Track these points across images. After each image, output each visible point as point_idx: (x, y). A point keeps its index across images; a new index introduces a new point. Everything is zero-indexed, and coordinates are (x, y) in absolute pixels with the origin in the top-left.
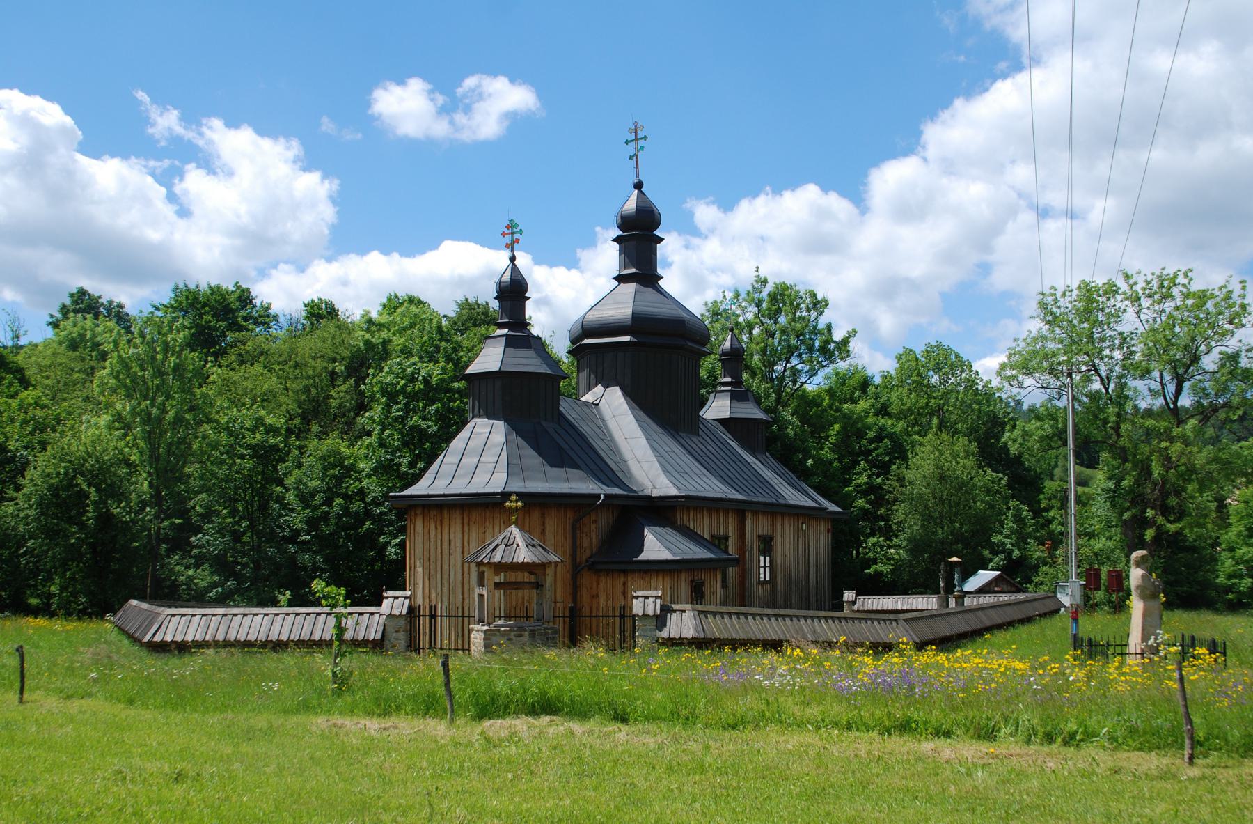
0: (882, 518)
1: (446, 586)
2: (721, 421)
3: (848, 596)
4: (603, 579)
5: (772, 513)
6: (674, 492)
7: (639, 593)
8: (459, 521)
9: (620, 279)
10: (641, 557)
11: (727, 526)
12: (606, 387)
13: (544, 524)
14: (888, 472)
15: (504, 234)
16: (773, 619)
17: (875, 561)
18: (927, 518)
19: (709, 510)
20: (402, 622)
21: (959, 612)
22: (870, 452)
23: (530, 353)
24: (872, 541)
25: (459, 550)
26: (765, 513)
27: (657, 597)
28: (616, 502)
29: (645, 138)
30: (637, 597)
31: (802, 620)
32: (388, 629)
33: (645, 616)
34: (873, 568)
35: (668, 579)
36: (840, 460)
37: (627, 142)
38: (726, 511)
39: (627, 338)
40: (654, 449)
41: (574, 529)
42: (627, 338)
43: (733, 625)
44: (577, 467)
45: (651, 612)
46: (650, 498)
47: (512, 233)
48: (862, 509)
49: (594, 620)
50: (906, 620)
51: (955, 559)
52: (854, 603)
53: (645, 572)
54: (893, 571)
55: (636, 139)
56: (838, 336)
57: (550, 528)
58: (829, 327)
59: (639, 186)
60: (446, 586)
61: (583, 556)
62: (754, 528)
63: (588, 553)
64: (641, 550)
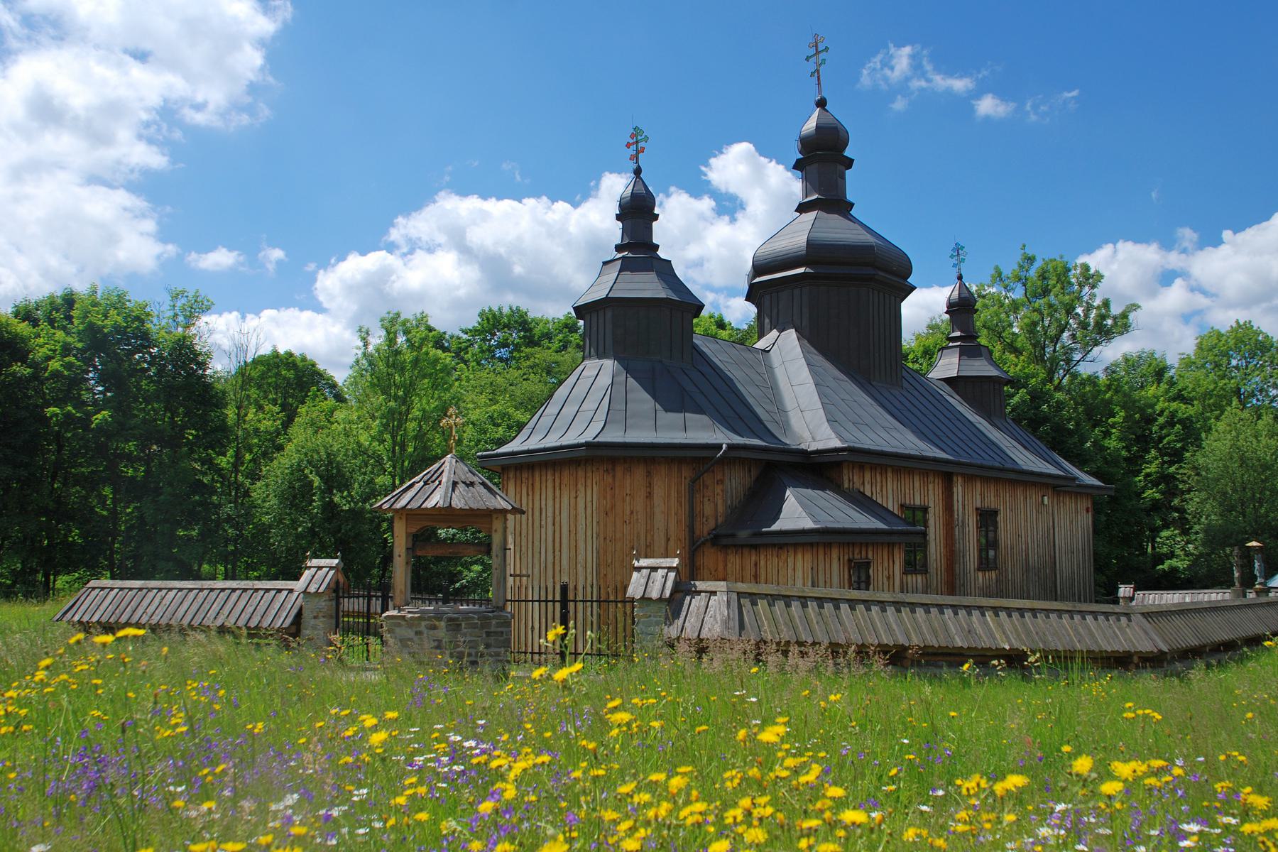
0: (1176, 510)
1: (537, 566)
2: (948, 381)
3: (1124, 590)
4: (731, 558)
5: (997, 480)
6: (836, 443)
7: (644, 562)
8: (550, 478)
9: (802, 208)
10: (776, 527)
11: (927, 494)
12: (781, 331)
13: (650, 485)
14: (1181, 460)
15: (628, 145)
16: (890, 610)
17: (1172, 555)
18: (1227, 508)
19: (897, 471)
20: (323, 604)
21: (1238, 607)
22: (1161, 439)
23: (652, 276)
24: (1165, 533)
25: (550, 520)
26: (986, 480)
27: (670, 569)
28: (743, 454)
29: (826, 49)
30: (639, 569)
31: (948, 613)
32: (306, 613)
33: (645, 599)
34: (1168, 563)
35: (808, 557)
36: (1127, 448)
37: (807, 59)
38: (924, 473)
39: (801, 270)
40: (821, 395)
41: (692, 492)
42: (801, 270)
43: (901, 622)
44: (700, 410)
45: (655, 594)
46: (804, 453)
47: (637, 142)
48: (1153, 500)
49: (543, 598)
50: (1146, 615)
51: (1254, 544)
52: (1132, 599)
53: (781, 546)
54: (1189, 567)
55: (817, 52)
56: (1116, 310)
57: (659, 490)
58: (1106, 304)
59: (821, 104)
60: (537, 566)
61: (704, 529)
62: (968, 499)
63: (712, 524)
64: (776, 517)
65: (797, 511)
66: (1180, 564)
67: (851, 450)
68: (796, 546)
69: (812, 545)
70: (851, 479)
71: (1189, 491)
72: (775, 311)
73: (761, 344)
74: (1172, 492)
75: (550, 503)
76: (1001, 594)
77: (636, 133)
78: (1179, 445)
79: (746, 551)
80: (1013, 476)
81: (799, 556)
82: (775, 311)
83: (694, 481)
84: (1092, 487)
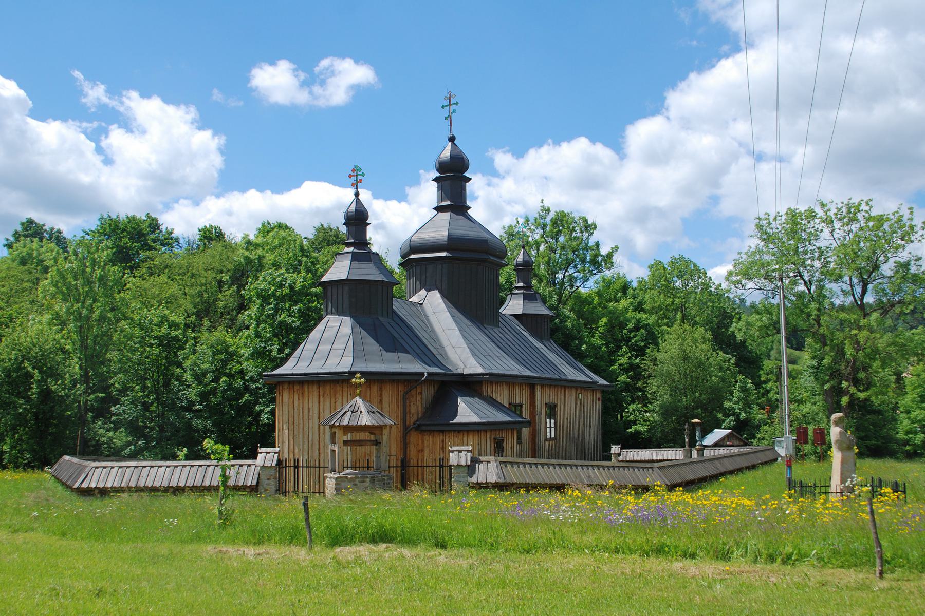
3: (615, 449)
4: (426, 437)
6: (480, 370)
7: (455, 448)
9: (439, 209)
11: (521, 396)
12: (428, 291)
14: (644, 354)
15: (350, 176)
16: (557, 468)
17: (635, 423)
18: (674, 389)
21: (700, 462)
22: (630, 339)
23: (370, 265)
24: (632, 407)
25: (316, 416)
27: (468, 451)
29: (457, 103)
30: (453, 451)
31: (580, 468)
35: (476, 438)
36: (607, 345)
37: (443, 107)
38: (521, 385)
39: (444, 254)
42: (444, 254)
44: (407, 352)
45: (463, 463)
46: (462, 375)
48: (625, 382)
50: (659, 468)
51: (696, 420)
52: (619, 455)
53: (459, 431)
55: (450, 104)
56: (604, 251)
58: (597, 245)
61: (411, 420)
63: (415, 418)
64: (455, 415)
65: (467, 411)
66: (642, 428)
67: (491, 375)
68: (468, 431)
69: (478, 431)
70: (488, 390)
71: (650, 376)
72: (423, 277)
73: (415, 299)
74: (637, 377)
75: (316, 405)
76: (556, 457)
77: (356, 169)
78: (643, 344)
79: (437, 434)
80: (565, 384)
81: (471, 437)
82: (423, 277)
83: (406, 393)
84: (604, 386)
